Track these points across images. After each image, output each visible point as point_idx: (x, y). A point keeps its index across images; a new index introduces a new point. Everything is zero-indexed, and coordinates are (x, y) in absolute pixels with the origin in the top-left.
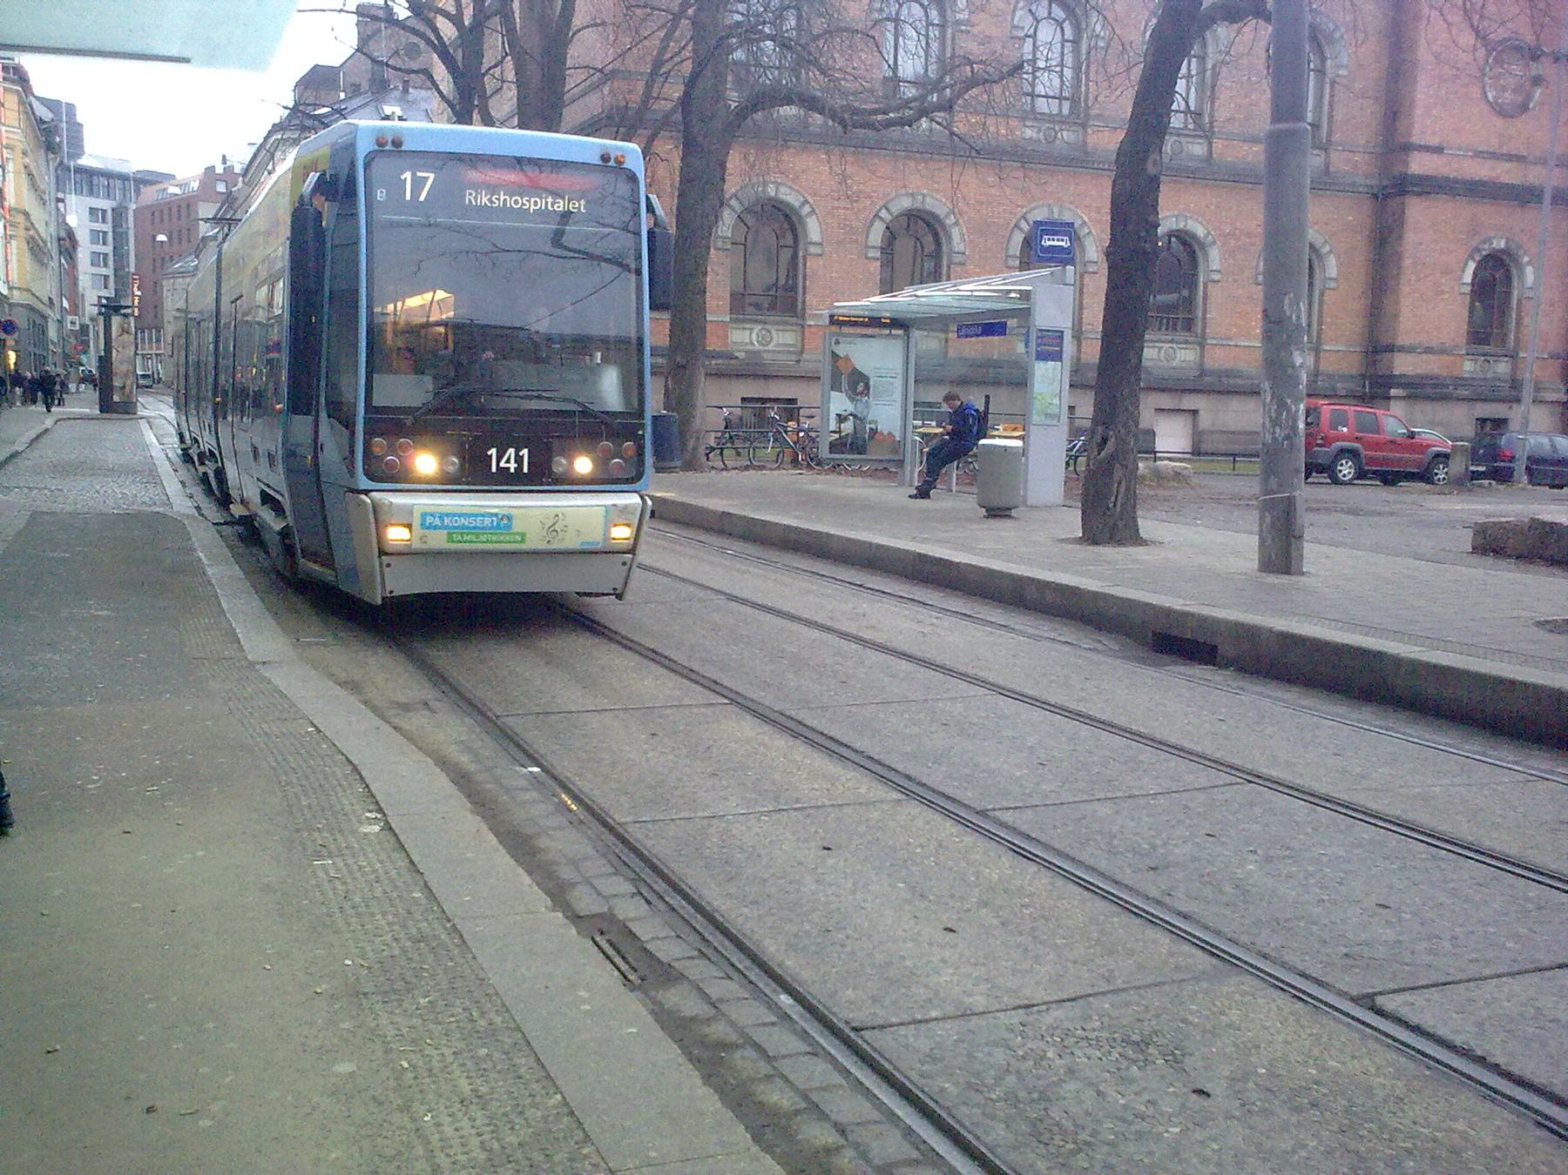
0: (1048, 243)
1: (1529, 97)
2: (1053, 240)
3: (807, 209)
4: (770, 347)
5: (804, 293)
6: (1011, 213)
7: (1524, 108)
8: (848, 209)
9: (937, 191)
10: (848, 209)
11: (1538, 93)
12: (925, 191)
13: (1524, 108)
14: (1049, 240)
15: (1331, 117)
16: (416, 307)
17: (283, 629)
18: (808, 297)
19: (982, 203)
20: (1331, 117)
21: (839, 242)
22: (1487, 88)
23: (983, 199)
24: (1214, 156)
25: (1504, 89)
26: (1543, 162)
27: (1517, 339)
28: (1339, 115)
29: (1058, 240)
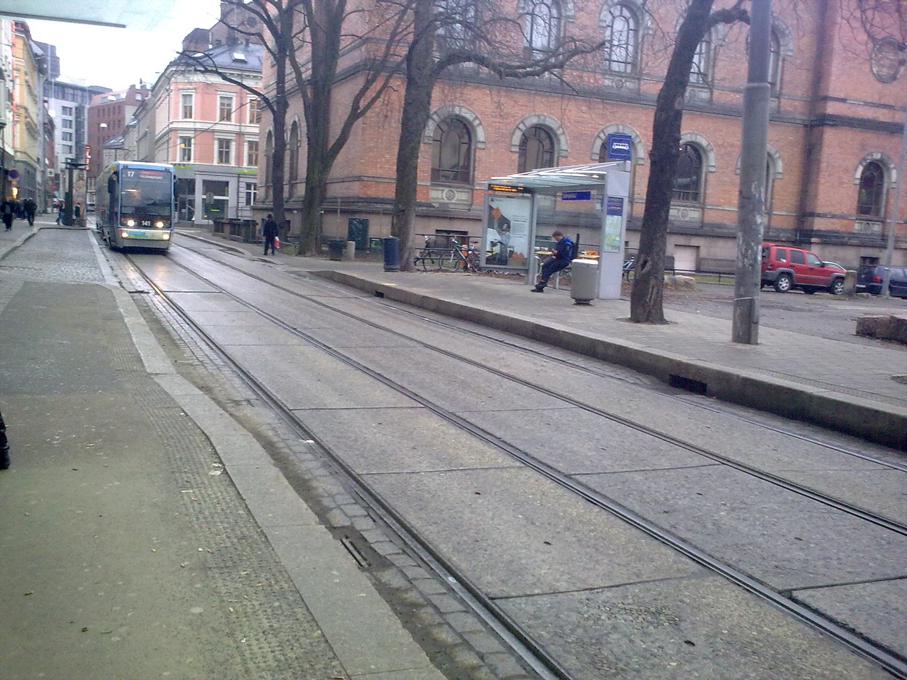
1: (896, 72)
3: (477, 122)
4: (453, 201)
5: (474, 170)
7: (894, 78)
18: (476, 173)
23: (580, 119)
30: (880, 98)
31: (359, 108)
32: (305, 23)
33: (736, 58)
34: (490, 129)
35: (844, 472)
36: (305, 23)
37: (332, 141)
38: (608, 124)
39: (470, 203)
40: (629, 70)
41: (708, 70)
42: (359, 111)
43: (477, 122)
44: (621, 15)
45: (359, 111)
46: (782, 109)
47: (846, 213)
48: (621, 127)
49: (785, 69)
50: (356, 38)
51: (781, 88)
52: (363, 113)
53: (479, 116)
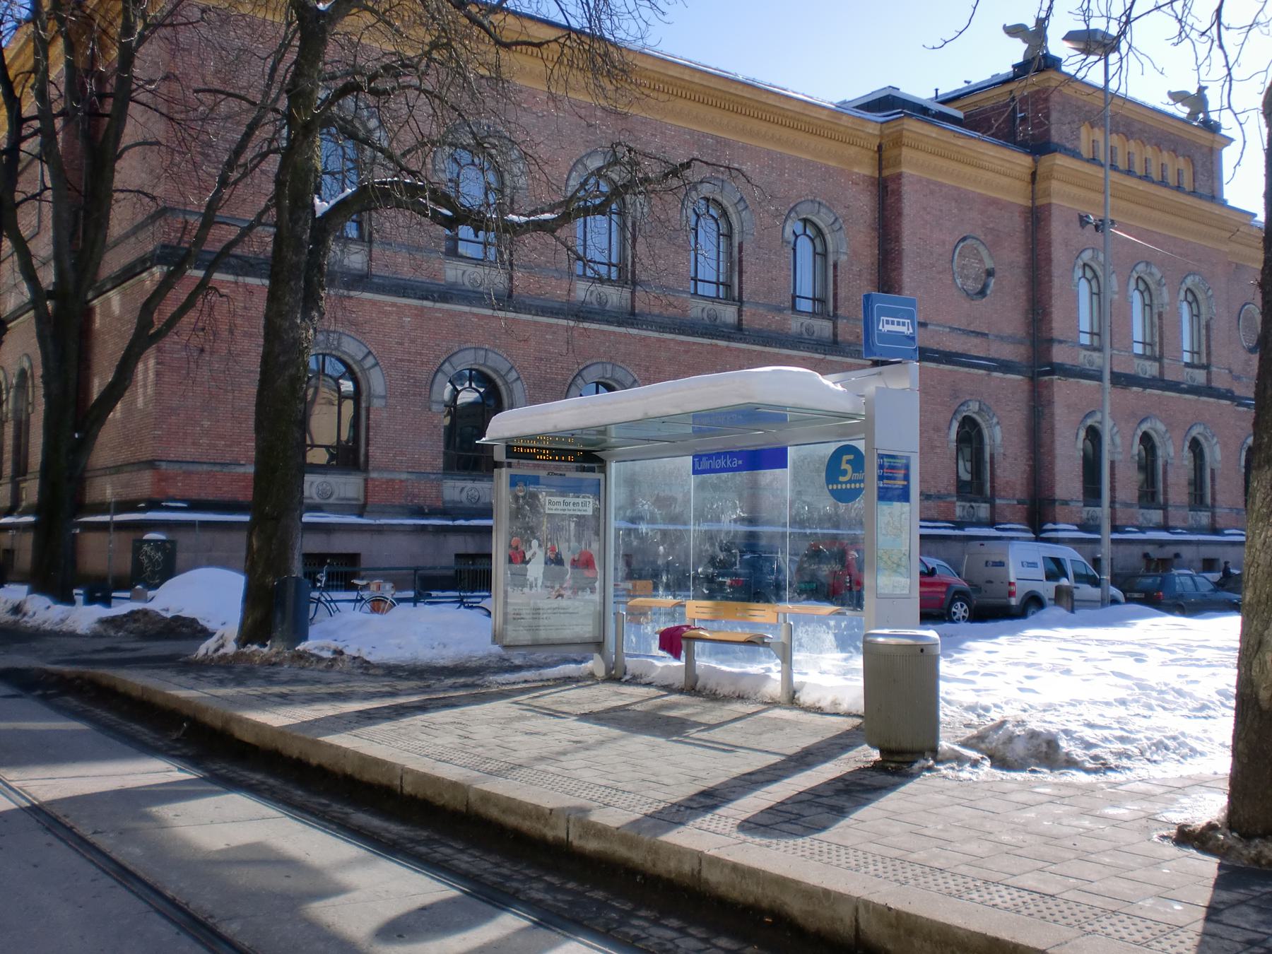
0: (888, 328)
1: (985, 286)
2: (893, 323)
3: (370, 361)
4: (331, 501)
5: (367, 444)
6: (568, 370)
7: (982, 293)
8: (411, 361)
9: (499, 347)
10: (411, 361)
11: (992, 281)
12: (487, 347)
13: (982, 293)
14: (888, 322)
15: (835, 295)
16: (840, 110)
17: (890, 909)
18: (371, 449)
19: (542, 359)
20: (835, 295)
21: (403, 394)
22: (956, 276)
23: (543, 355)
24: (744, 322)
25: (967, 277)
26: (1001, 338)
27: (993, 487)
28: (842, 293)
29: (898, 323)
30: (968, 325)
31: (151, 324)
32: (43, 181)
33: (770, 260)
34: (393, 373)
35: (200, 95)
36: (43, 181)
37: (97, 387)
38: (588, 363)
39: (362, 502)
40: (614, 275)
41: (731, 277)
42: (152, 331)
43: (370, 361)
44: (805, 233)
45: (152, 331)
46: (839, 339)
47: (943, 491)
48: (609, 367)
49: (839, 278)
50: (245, 105)
51: (835, 308)
52: (160, 335)
53: (373, 351)
